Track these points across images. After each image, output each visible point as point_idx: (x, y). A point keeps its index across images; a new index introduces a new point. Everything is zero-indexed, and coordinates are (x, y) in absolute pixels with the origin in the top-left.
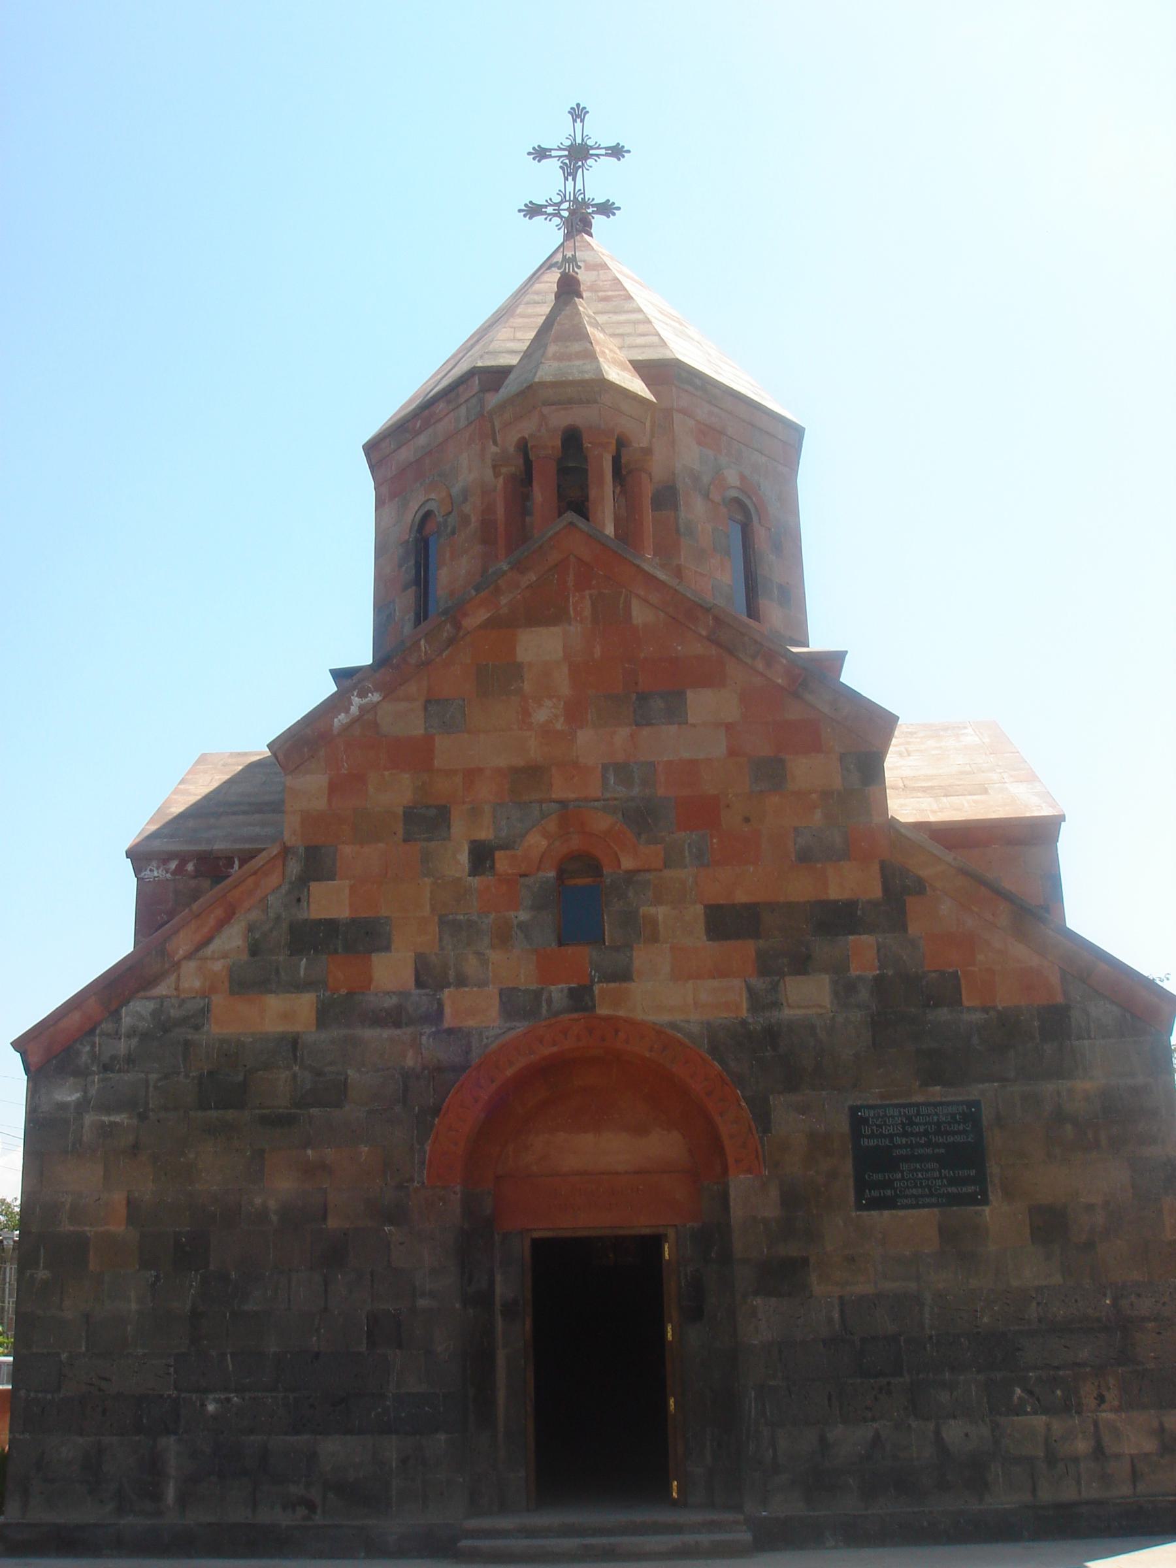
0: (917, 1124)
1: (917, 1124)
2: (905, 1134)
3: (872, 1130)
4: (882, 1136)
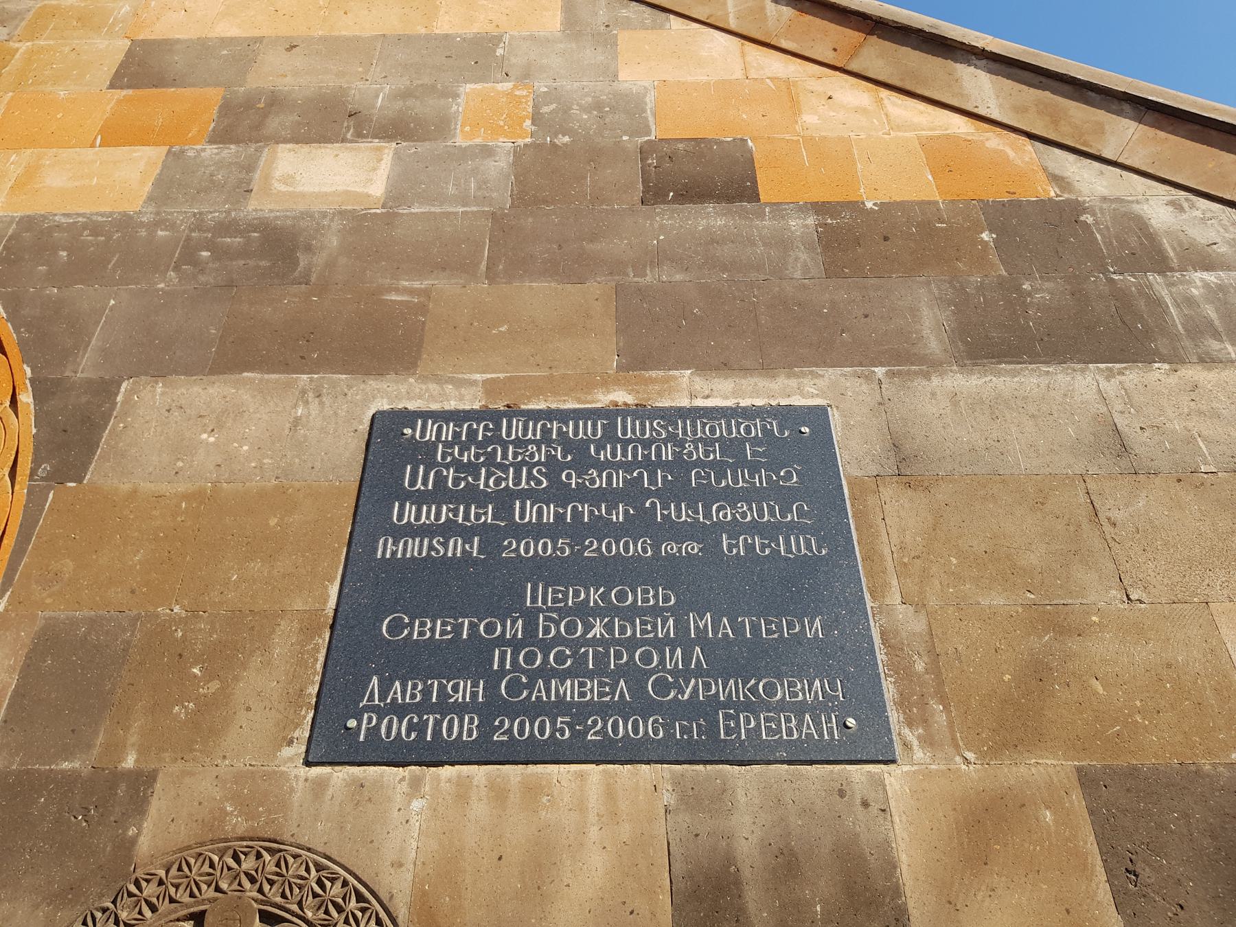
0: (601, 466)
1: (601, 466)
2: (559, 494)
3: (440, 480)
4: (472, 496)
